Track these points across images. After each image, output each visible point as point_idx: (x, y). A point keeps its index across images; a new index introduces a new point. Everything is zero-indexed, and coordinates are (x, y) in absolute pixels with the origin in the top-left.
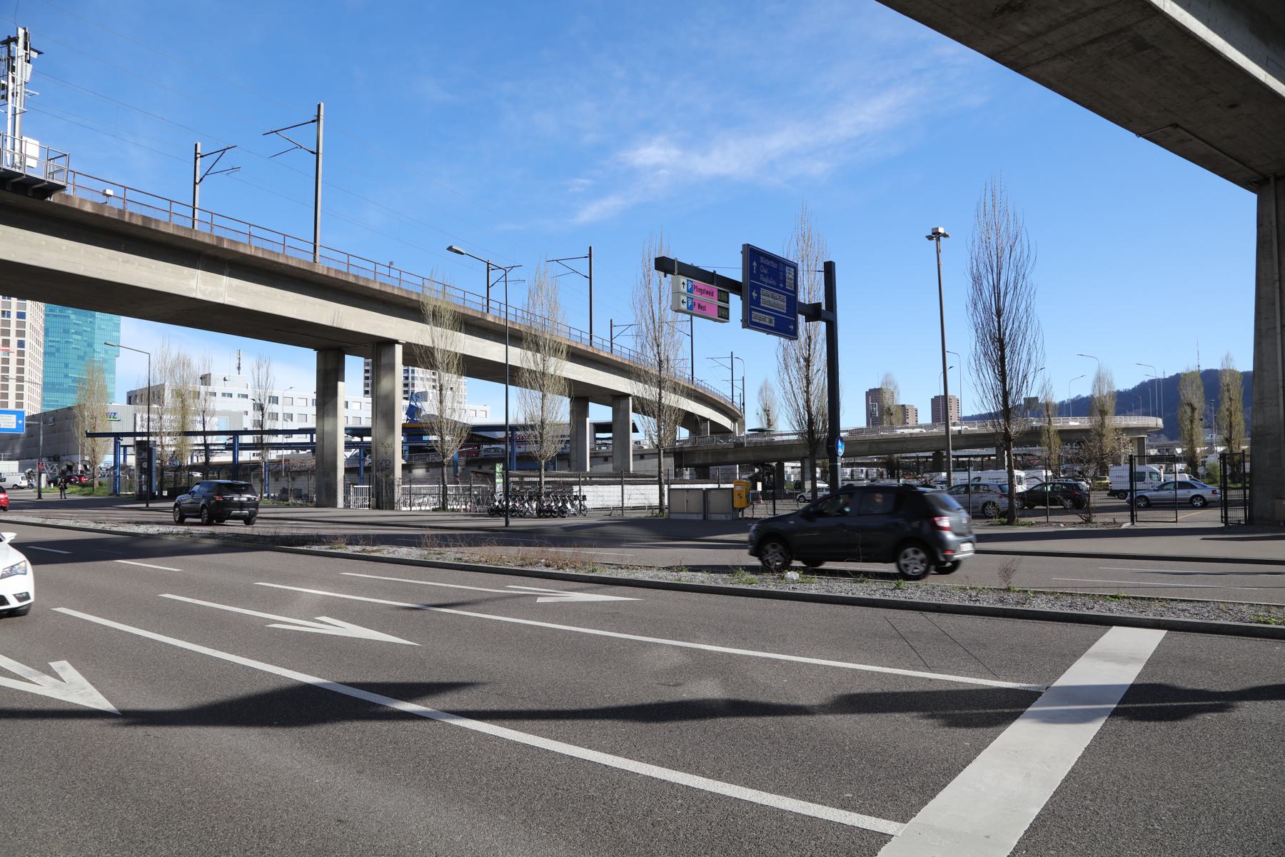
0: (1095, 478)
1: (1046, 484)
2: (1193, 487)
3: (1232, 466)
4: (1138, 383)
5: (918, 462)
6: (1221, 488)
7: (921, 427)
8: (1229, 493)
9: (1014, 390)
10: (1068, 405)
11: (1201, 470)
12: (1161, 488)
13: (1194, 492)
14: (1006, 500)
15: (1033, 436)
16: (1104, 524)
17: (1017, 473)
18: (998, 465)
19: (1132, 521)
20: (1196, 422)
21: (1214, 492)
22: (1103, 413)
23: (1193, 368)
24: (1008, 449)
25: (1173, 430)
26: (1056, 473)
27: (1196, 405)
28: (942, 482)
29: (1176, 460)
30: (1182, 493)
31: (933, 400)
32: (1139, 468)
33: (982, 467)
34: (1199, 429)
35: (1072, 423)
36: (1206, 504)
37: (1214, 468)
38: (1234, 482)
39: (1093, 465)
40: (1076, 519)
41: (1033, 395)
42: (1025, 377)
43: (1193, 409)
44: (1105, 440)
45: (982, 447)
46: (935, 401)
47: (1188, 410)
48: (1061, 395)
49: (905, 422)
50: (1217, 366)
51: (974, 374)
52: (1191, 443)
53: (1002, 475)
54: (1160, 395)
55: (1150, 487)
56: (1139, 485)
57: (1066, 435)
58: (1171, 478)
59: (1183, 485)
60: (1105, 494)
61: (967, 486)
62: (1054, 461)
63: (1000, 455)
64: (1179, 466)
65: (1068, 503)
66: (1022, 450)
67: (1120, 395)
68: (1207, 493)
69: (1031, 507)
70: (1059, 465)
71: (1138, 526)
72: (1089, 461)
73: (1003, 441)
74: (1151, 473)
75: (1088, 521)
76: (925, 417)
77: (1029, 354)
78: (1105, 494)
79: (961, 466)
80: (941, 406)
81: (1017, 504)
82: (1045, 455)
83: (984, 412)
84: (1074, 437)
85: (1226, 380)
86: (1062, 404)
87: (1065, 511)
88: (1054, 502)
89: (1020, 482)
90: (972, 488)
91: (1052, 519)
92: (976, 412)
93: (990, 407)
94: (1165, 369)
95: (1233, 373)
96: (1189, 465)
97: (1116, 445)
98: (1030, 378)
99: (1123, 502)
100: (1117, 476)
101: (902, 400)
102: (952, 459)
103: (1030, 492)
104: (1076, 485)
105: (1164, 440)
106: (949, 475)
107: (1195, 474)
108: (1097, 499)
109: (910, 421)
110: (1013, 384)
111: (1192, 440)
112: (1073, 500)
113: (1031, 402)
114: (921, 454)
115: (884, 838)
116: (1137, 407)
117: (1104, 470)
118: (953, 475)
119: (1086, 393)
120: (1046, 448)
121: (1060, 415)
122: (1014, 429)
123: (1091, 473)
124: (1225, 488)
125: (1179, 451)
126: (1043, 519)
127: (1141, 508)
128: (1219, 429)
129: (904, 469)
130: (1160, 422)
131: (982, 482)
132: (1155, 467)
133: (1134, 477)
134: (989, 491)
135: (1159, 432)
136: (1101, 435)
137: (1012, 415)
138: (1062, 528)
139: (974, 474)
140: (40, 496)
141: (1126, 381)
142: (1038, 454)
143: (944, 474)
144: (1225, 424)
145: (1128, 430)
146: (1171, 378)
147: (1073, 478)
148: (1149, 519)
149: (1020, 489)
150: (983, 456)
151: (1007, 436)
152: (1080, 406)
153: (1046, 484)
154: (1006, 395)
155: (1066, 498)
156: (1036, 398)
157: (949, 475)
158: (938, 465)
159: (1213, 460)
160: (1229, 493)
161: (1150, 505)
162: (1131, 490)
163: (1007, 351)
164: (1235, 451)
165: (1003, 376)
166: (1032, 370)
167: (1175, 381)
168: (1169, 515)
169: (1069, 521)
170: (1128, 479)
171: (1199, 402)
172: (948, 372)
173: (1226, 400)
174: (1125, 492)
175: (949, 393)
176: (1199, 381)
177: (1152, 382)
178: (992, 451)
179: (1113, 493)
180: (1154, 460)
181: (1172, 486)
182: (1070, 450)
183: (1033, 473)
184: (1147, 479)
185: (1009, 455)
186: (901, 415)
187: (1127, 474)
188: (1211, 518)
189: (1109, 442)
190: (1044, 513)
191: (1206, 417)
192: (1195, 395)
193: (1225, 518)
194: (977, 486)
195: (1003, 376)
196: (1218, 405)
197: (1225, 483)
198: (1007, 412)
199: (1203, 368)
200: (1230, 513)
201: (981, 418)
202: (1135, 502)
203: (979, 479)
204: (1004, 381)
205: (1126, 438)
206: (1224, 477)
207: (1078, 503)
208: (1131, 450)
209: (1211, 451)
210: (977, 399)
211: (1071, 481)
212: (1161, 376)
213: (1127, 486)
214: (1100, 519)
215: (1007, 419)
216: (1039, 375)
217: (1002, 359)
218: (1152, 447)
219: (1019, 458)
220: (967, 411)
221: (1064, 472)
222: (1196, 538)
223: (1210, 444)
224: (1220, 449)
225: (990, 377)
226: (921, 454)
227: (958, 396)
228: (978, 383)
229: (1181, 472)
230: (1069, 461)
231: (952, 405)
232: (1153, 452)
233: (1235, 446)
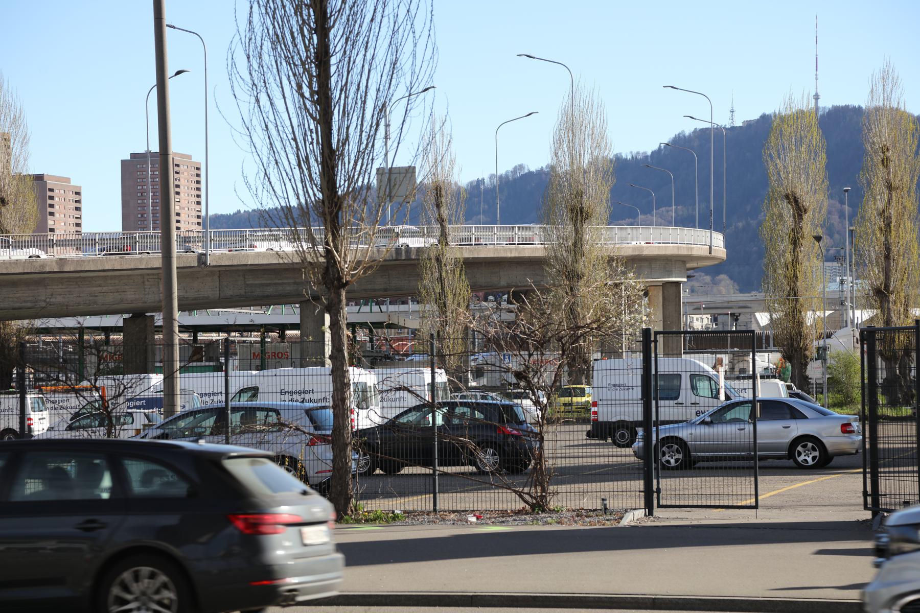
0: (555, 389)
1: (431, 407)
2: (796, 415)
3: (890, 359)
4: (666, 137)
5: (80, 344)
6: (863, 418)
7: (90, 241)
8: (884, 430)
9: (352, 147)
10: (490, 192)
11: (814, 371)
12: (718, 417)
13: (798, 428)
14: (325, 452)
15: (399, 276)
16: (579, 513)
17: (358, 375)
18: (307, 355)
19: (649, 506)
20: (807, 244)
21: (846, 428)
22: (579, 215)
23: (802, 102)
24: (334, 309)
25: (747, 263)
27: (807, 201)
28: (151, 403)
29: (752, 342)
31: (124, 163)
32: (665, 365)
33: (262, 359)
36: (827, 461)
37: (847, 365)
38: (893, 403)
39: (553, 356)
40: (507, 500)
41: (402, 161)
42: (382, 110)
43: (800, 211)
45: (264, 301)
46: (132, 168)
47: (787, 210)
48: (473, 163)
49: (42, 227)
51: (246, 97)
53: (317, 381)
54: (715, 172)
55: (689, 413)
56: (666, 410)
57: (484, 274)
58: (743, 390)
59: (773, 409)
61: (221, 414)
64: (765, 360)
65: (488, 458)
66: (368, 313)
67: (623, 169)
68: (828, 430)
69: (392, 469)
70: (465, 355)
71: (664, 517)
72: (541, 345)
73: (323, 285)
75: (539, 506)
76: (104, 214)
77: (395, 47)
79: (203, 356)
80: (150, 180)
81: (355, 460)
82: (428, 327)
83: (270, 203)
84: (504, 278)
85: (883, 134)
86: (476, 186)
87: (479, 481)
88: (451, 456)
89: (363, 403)
90: (235, 419)
91: (446, 501)
92: (249, 204)
94: (736, 105)
95: (897, 116)
96: (787, 357)
97: (609, 301)
98: (395, 115)
99: (626, 455)
100: (613, 388)
101: (34, 163)
102: (179, 336)
103: (390, 427)
104: (509, 409)
105: (726, 291)
106: (169, 381)
107: (801, 381)
108: (563, 445)
109: (61, 225)
110: (349, 128)
111: (795, 292)
112: (499, 448)
113: (396, 179)
115: (70, 428)
116: (664, 202)
117: (578, 368)
118: (182, 381)
119: (537, 158)
120: (431, 307)
121: (469, 217)
122: (357, 250)
123: (547, 377)
124: (871, 419)
125: (763, 319)
126: (422, 502)
128: (860, 265)
130: (718, 240)
131: (262, 401)
132: (703, 362)
133: (654, 387)
134: (281, 425)
135: (716, 269)
136: (573, 276)
137: (345, 216)
138: (473, 527)
139: (240, 379)
141: (638, 131)
143: (156, 379)
144: (874, 251)
145: (637, 262)
146: (749, 125)
147: (502, 389)
148: (690, 498)
149: (365, 419)
152: (520, 196)
153: (431, 407)
154: (330, 158)
155: (483, 444)
157: (169, 381)
158: (138, 349)
159: (845, 344)
161: (692, 462)
162: (647, 423)
163: (336, 35)
164: (898, 321)
166: (401, 91)
167: (761, 131)
168: (738, 487)
169: (488, 507)
170: (638, 393)
171: (815, 198)
172: (172, 85)
173: (879, 187)
174: (629, 427)
175: (175, 147)
176: (815, 136)
177: (702, 135)
178: (289, 314)
179: (603, 431)
180: (702, 342)
181: (743, 413)
182: (495, 314)
183: (398, 375)
184: (686, 395)
185: (335, 326)
186: (30, 207)
187: (636, 379)
188: (837, 496)
189: (592, 297)
190: (428, 486)
192: (802, 173)
194: (249, 413)
196: (857, 199)
197: (874, 404)
198: (332, 209)
199: (827, 103)
200: (886, 485)
201: (264, 220)
202: (659, 456)
203: (254, 391)
204: (325, 120)
205: (634, 281)
206: (870, 389)
207: (512, 456)
208: (649, 316)
209: (840, 322)
210: (253, 169)
212: (723, 121)
213: (635, 413)
214: (567, 499)
216: (420, 105)
217: (322, 56)
218: (697, 309)
219: (362, 336)
220: (225, 199)
221: (479, 373)
222: (805, 550)
224: (862, 316)
225: (288, 106)
227: (198, 158)
230: (492, 343)
231: (183, 182)
232: (700, 322)
233: (896, 308)
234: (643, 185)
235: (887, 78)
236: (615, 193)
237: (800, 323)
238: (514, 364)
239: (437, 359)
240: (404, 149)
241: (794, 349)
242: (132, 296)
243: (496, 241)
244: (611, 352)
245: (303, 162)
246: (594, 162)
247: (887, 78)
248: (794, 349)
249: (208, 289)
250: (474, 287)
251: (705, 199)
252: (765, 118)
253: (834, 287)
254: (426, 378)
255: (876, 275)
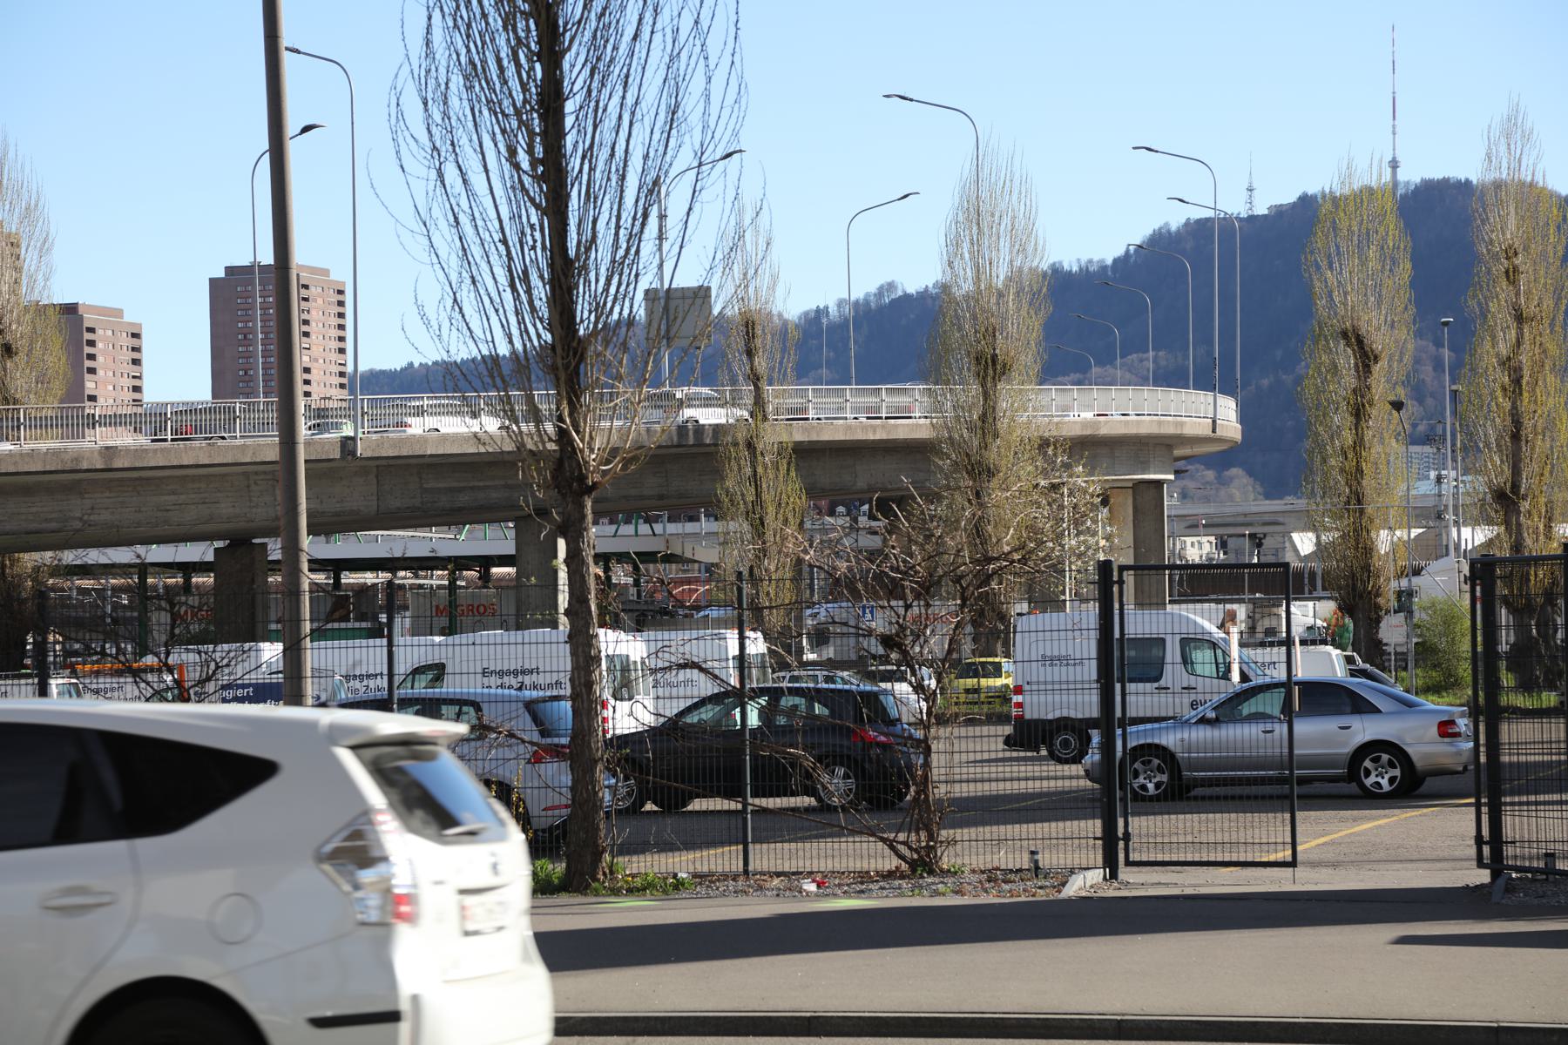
0: (952, 664)
1: (739, 696)
2: (1361, 706)
3: (1521, 611)
4: (1139, 234)
5: (142, 593)
6: (1474, 712)
8: (1511, 732)
9: (602, 255)
10: (839, 329)
11: (1393, 631)
12: (1229, 710)
13: (1364, 730)
14: (559, 774)
15: (684, 473)
16: (992, 876)
17: (614, 643)
18: (525, 608)
19: (1110, 863)
20: (1379, 413)
21: (1446, 729)
22: (990, 368)
23: (1371, 174)
24: (573, 530)
25: (1279, 448)
26: (784, 645)
27: (1379, 341)
29: (1286, 582)
30: (1322, 736)
32: (1138, 623)
33: (451, 616)
34: (1387, 447)
35: (416, 427)
36: (1414, 785)
37: (1449, 621)
38: (1526, 686)
39: (945, 607)
40: (871, 855)
41: (687, 278)
42: (653, 189)
43: (1366, 358)
44: (996, 495)
45: (453, 517)
47: (1346, 359)
48: (809, 279)
49: (75, 393)
50: (1466, 166)
51: (420, 168)
52: (1355, 509)
53: (543, 653)
54: (1221, 293)
55: (1181, 705)
56: (1139, 699)
57: (829, 469)
58: (1271, 665)
59: (1322, 697)
60: (993, 739)
62: (776, 591)
63: (531, 557)
64: (1306, 614)
65: (836, 783)
66: (632, 536)
68: (1420, 726)
69: (673, 803)
70: (798, 606)
71: (1137, 883)
72: (927, 590)
73: (548, 492)
74: (1189, 643)
75: (923, 865)
76: (180, 371)
77: (674, 85)
78: (993, 739)
80: (259, 313)
81: (609, 788)
82: (734, 559)
83: (463, 351)
84: (864, 475)
85: (1507, 228)
87: (821, 822)
88: (774, 779)
89: (624, 689)
91: (765, 857)
92: (429, 353)
93: (498, 328)
94: (1256, 178)
96: (1346, 608)
97: (1041, 515)
98: (676, 199)
99: (1072, 777)
100: (1049, 662)
101: (61, 286)
103: (669, 731)
105: (1242, 496)
106: (293, 655)
107: (1370, 648)
108: (963, 761)
109: (107, 389)
110: (598, 223)
112: (856, 767)
113: (677, 308)
114: (158, 553)
116: (1135, 345)
117: (990, 630)
119: (918, 272)
120: (738, 526)
121: (804, 372)
122: (611, 428)
123: (936, 644)
124: (1489, 712)
125: (1304, 543)
126: (723, 859)
127: (1145, 803)
128: (1469, 452)
129: (64, 626)
130: (1227, 410)
132: (1203, 618)
133: (1120, 660)
135: (1223, 458)
136: (980, 471)
137: (591, 371)
138: (812, 901)
140: (1214, 431)
141: (1090, 223)
142: (708, 554)
143: (271, 652)
144: (1492, 429)
145: (1090, 448)
146: (1279, 213)
147: (859, 665)
148: (1183, 849)
149: (627, 717)
150: (458, 564)
151: (565, 470)
152: (891, 336)
153: (739, 696)
154: (564, 273)
155: (828, 760)
156: (701, 294)
157: (293, 655)
159: (1444, 584)
160: (1511, 732)
161: (1185, 787)
162: (1108, 720)
165: (552, 177)
167: (1303, 218)
168: (1262, 831)
169: (836, 867)
170: (1091, 670)
171: (1391, 334)
175: (301, 255)
176: (1392, 230)
177: (1199, 230)
178: (497, 539)
179: (1033, 736)
180: (1201, 583)
181: (1271, 704)
182: (848, 538)
183: (682, 643)
184: (1173, 673)
185: (575, 560)
186: (55, 359)
187: (1087, 647)
188: (1431, 844)
189: (1012, 507)
190: (733, 831)
191: (1419, 393)
192: (1369, 293)
193: (1492, 846)
195: (552, 177)
196: (1464, 336)
198: (565, 358)
199: (1412, 174)
200: (1513, 825)
201: (454, 381)
202: (1128, 778)
204: (556, 209)
205: (1084, 480)
206: (1486, 662)
207: (876, 778)
208: (1108, 539)
209: (1435, 547)
210: (433, 293)
211: (848, 681)
212: (1235, 205)
213: (1086, 705)
214: (971, 852)
215: (571, 385)
216: (717, 183)
217: (551, 99)
218: (1193, 527)
219: (621, 576)
220: (385, 346)
221: (820, 638)
222: (1372, 939)
223: (1434, 516)
224: (1473, 537)
225: (492, 183)
226: (158, 553)
227: (341, 274)
228: (440, 214)
229: (1313, 638)
230: (840, 587)
231: (315, 315)
232: (1198, 549)
233: (1531, 524)
234: (1096, 317)
235: (1513, 130)
236: (1053, 331)
237: (1368, 550)
238: (880, 623)
239: (747, 615)
240: (690, 255)
241: (1357, 594)
242: (229, 510)
243: (844, 413)
244: (1047, 601)
245: (518, 280)
246: (1015, 277)
247: (1513, 130)
248: (1357, 594)
249: (359, 497)
250: (812, 492)
251: (1205, 339)
252: (1306, 203)
253: (1425, 487)
254: (731, 648)
255: (1496, 467)
